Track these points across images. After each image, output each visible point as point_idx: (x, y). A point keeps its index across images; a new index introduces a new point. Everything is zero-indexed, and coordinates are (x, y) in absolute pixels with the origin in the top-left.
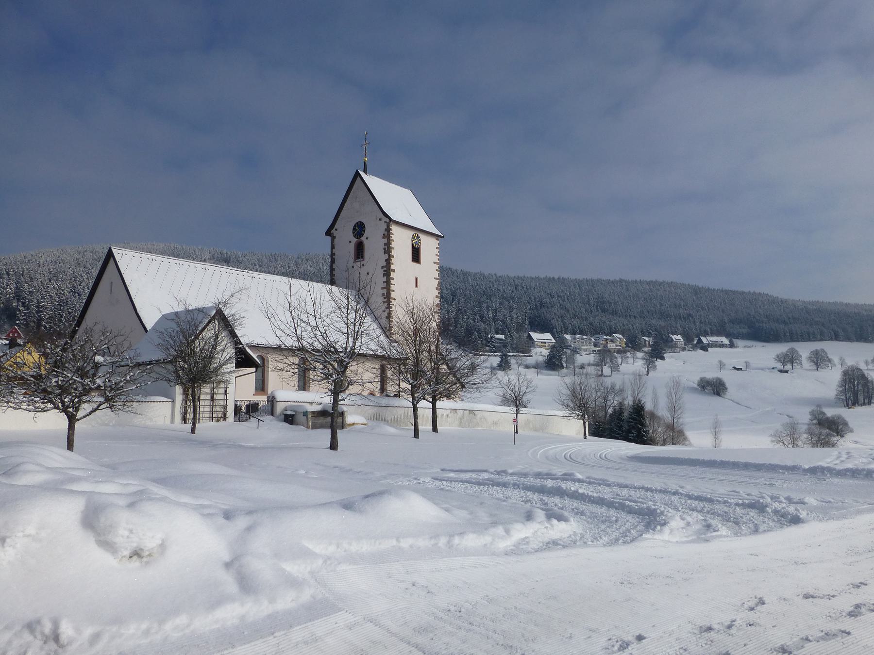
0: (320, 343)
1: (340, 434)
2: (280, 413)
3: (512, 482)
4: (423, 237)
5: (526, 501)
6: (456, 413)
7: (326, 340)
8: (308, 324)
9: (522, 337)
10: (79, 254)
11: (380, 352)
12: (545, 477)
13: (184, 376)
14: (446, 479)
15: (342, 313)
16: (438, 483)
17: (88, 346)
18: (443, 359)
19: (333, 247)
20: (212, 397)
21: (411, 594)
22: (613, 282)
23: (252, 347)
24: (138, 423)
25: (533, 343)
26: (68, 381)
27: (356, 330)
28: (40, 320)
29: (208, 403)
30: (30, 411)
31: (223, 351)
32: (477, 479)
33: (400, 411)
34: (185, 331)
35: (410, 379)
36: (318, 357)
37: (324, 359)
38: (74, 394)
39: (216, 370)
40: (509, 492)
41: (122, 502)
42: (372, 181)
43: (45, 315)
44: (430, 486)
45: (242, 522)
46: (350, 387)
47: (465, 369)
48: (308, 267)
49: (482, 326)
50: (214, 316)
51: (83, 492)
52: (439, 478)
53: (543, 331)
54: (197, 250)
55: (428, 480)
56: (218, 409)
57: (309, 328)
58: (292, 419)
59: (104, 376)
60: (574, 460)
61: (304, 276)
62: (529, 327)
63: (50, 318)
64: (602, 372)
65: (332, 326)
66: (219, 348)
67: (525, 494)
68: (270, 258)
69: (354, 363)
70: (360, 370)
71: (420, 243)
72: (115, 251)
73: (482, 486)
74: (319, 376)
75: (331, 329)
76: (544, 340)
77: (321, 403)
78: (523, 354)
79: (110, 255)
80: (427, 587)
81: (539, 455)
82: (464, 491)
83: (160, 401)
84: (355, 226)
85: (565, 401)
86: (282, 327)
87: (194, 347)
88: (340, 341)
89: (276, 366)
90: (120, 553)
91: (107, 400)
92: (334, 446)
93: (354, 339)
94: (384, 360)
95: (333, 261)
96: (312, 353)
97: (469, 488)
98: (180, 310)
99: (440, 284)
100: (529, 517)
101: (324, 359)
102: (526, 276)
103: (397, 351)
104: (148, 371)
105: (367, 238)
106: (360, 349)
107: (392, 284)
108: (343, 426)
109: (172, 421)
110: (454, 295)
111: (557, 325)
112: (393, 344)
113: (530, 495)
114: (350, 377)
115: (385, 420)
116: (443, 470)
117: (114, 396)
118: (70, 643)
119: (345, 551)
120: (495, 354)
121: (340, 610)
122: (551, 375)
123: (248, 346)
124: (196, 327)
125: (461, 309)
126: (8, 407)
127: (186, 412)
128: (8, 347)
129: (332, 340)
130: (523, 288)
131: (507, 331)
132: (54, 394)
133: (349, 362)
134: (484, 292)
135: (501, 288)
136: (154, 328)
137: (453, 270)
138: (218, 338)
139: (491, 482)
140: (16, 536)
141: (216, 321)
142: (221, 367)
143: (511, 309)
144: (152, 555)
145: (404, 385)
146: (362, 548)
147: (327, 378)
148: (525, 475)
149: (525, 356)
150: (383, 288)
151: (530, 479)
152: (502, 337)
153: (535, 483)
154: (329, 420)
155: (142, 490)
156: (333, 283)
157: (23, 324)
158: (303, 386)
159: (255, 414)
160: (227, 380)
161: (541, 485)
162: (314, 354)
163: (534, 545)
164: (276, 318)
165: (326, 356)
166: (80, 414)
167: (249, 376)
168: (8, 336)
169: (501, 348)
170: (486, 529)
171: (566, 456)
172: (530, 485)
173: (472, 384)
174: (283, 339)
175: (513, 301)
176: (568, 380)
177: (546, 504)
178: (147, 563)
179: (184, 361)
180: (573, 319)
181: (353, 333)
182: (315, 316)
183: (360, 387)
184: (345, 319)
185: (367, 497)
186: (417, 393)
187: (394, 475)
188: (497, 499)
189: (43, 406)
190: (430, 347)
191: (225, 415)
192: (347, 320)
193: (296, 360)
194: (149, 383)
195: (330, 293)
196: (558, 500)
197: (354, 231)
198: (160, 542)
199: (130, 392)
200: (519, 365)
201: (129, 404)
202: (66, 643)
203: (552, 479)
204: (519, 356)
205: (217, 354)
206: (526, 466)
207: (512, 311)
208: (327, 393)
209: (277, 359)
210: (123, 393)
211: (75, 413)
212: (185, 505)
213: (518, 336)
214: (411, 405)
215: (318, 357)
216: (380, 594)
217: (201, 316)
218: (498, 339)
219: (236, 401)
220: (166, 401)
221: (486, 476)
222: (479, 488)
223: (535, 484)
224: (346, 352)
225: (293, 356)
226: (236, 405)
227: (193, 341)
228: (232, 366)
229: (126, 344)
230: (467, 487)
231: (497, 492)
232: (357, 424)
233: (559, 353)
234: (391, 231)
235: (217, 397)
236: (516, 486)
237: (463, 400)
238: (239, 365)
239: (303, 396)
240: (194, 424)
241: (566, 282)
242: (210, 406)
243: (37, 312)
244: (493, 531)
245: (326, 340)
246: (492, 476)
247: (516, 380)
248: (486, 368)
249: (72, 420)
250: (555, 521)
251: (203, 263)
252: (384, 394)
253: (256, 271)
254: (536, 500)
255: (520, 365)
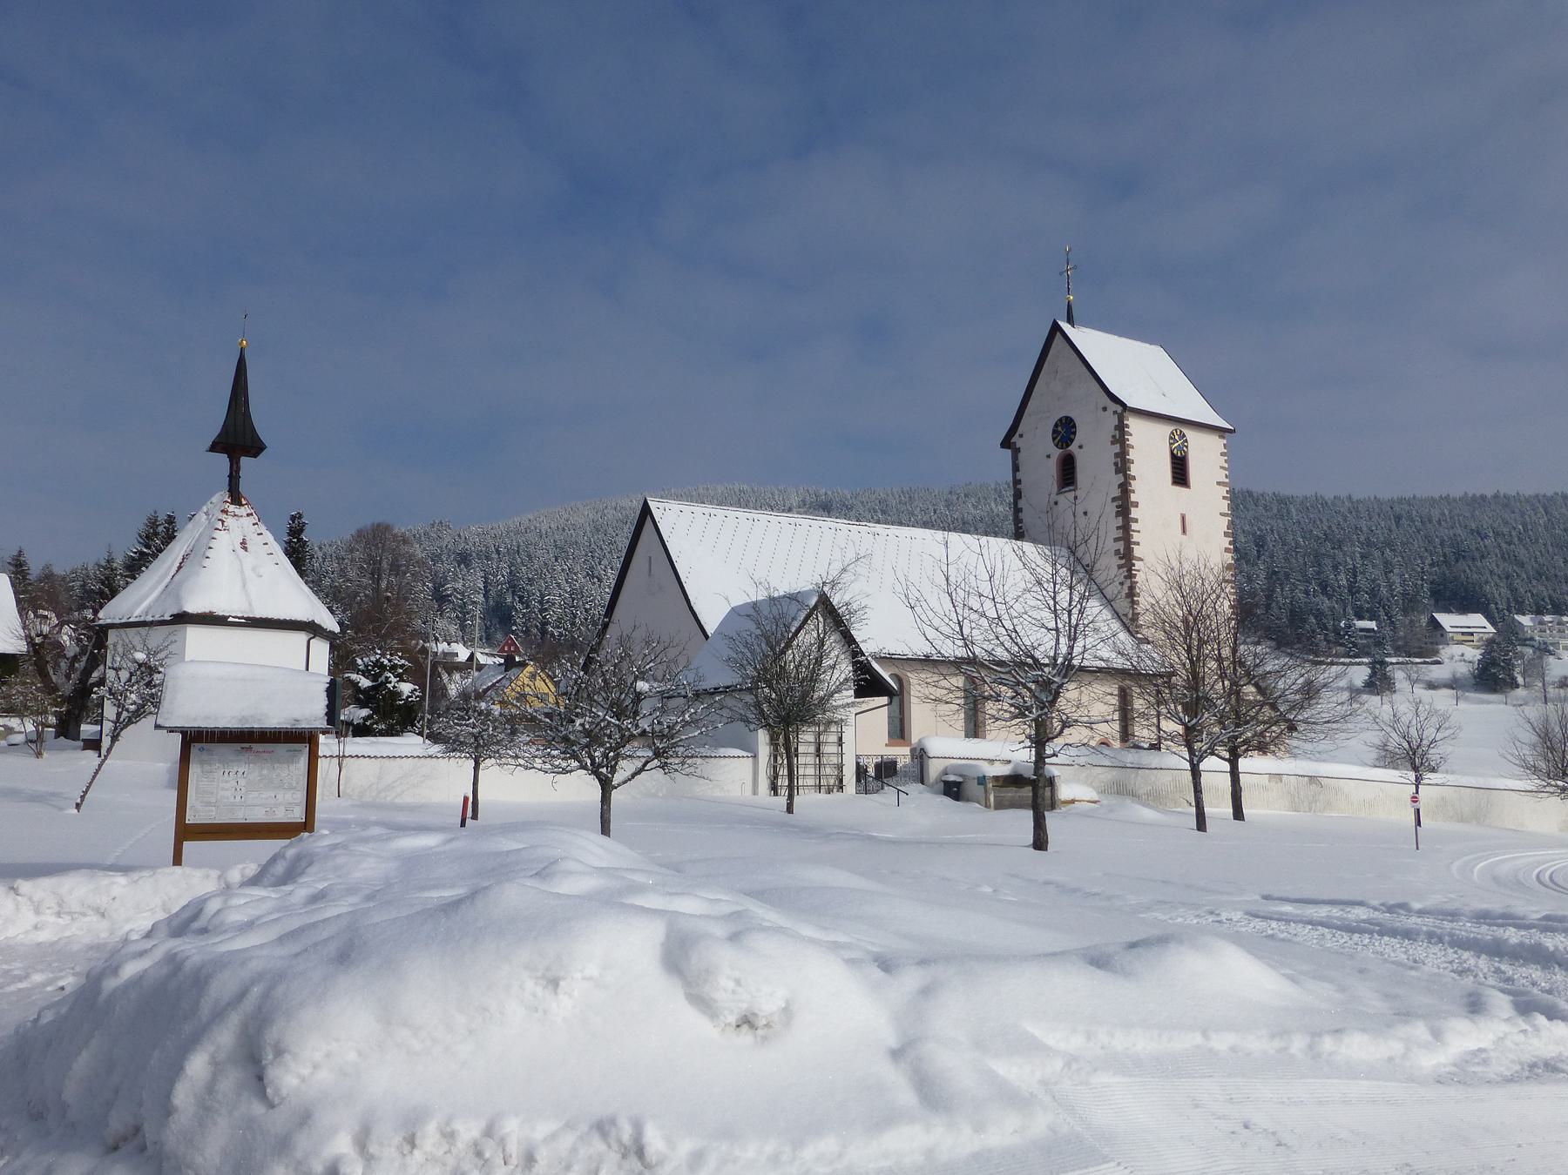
0: (1006, 649)
1: (1051, 820)
2: (936, 779)
3: (1425, 928)
4: (1190, 434)
5: (1462, 972)
6: (1281, 781)
7: (1017, 644)
8: (983, 615)
9: (1417, 625)
10: (597, 513)
11: (1119, 663)
12: (1500, 921)
13: (771, 713)
14: (1276, 916)
15: (1045, 593)
16: (1259, 924)
17: (625, 665)
18: (1248, 674)
19: (1016, 468)
20: (818, 750)
21: (1244, 1145)
23: (888, 660)
24: (701, 794)
25: (1442, 635)
26: (599, 724)
27: (1074, 622)
28: (545, 623)
29: (811, 760)
30: (547, 772)
31: (833, 667)
32: (1345, 919)
33: (1164, 778)
34: (769, 633)
35: (1181, 715)
36: (1003, 676)
37: (1015, 678)
38: (608, 745)
39: (823, 701)
40: (1419, 950)
41: (720, 930)
42: (1085, 338)
43: (551, 616)
44: (1243, 929)
45: (911, 979)
46: (1066, 731)
47: (1297, 692)
48: (970, 511)
49: (1325, 603)
50: (815, 607)
51: (663, 911)
52: (1262, 914)
53: (1464, 609)
54: (776, 492)
55: (1237, 916)
56: (828, 771)
57: (984, 622)
58: (959, 790)
59: (651, 714)
60: (1562, 888)
61: (964, 527)
62: (1432, 602)
63: (559, 620)
65: (1025, 616)
66: (826, 663)
67: (1456, 956)
68: (900, 496)
69: (1071, 686)
70: (1085, 699)
71: (1187, 447)
72: (652, 505)
73: (1357, 935)
74: (1006, 711)
75: (1025, 622)
76: (1469, 627)
77: (1010, 761)
78: (1422, 660)
79: (646, 512)
80: (1274, 1133)
81: (1475, 874)
82: (1317, 943)
83: (734, 757)
84: (1056, 425)
85: (1530, 759)
86: (936, 622)
87: (785, 662)
88: (1044, 645)
89: (927, 692)
90: (722, 1018)
91: (657, 754)
92: (1040, 843)
93: (1070, 640)
94: (1126, 679)
95: (1018, 495)
96: (993, 669)
97: (1329, 936)
98: (760, 598)
99: (1231, 524)
100: (1475, 1006)
101: (1015, 678)
102: (1418, 496)
103: (1153, 659)
104: (717, 705)
105: (1081, 447)
106: (1083, 658)
107: (1134, 531)
108: (1053, 806)
109: (755, 792)
110: (1260, 543)
111: (1497, 596)
112: (1144, 647)
113: (1468, 959)
114: (1066, 712)
115: (1133, 795)
116: (1266, 898)
117: (668, 747)
118: (660, 1163)
119: (1102, 1048)
120: (1358, 660)
121: (1105, 1159)
122: (1489, 702)
123: (875, 659)
124: (787, 627)
125: (1279, 572)
126: (517, 765)
127: (776, 776)
128: (503, 668)
129: (1028, 643)
130: (1413, 521)
131: (1382, 613)
132: (580, 744)
133: (1063, 684)
134: (1325, 534)
135: (1363, 524)
136: (718, 631)
137: (1255, 495)
138: (823, 646)
139: (1377, 928)
140: (572, 978)
141: (819, 615)
142: (832, 696)
143: (1388, 568)
144: (771, 1026)
145: (1170, 726)
146: (1134, 1045)
147: (1022, 715)
148: (1454, 915)
149: (1425, 663)
150: (1116, 540)
151: (1464, 925)
152: (1372, 625)
153: (1478, 934)
154: (1027, 792)
155: (739, 911)
156: (1019, 535)
157: (522, 631)
158: (975, 729)
159: (891, 781)
160: (842, 720)
161: (1493, 940)
162: (996, 671)
163: (1502, 1066)
164: (924, 604)
165: (1018, 674)
166: (617, 778)
167: (877, 712)
168: (502, 650)
169: (1369, 648)
170: (1389, 1026)
171: (1542, 878)
172: (1467, 937)
173: (1314, 723)
174: (938, 643)
175: (1391, 550)
176: (1534, 711)
177: (1509, 980)
178: (765, 1038)
179: (770, 687)
180: (1534, 582)
181: (1067, 628)
182: (994, 599)
183: (1086, 732)
184: (1051, 603)
185: (1133, 945)
186: (1198, 741)
187: (1165, 903)
188: (1393, 963)
189: (564, 764)
190: (1219, 650)
191: (841, 781)
192: (1055, 603)
193: (959, 681)
194: (720, 725)
195: (1021, 557)
196: (1539, 973)
197: (1055, 436)
198: (783, 1006)
199: (692, 741)
200: (1413, 682)
201: (689, 761)
202: (654, 1162)
203: (1519, 927)
204: (1412, 663)
205: (824, 673)
206: (1453, 896)
207: (1392, 571)
208: (1023, 742)
209: (929, 680)
210: (680, 743)
211: (610, 775)
212: (812, 941)
213: (1407, 622)
214: (1187, 766)
215: (1003, 676)
216: (1182, 1137)
217: (794, 606)
218: (1362, 630)
219: (858, 757)
220: (743, 757)
221: (1360, 913)
222: (1351, 939)
223: (1479, 936)
224: (1054, 665)
225: (956, 675)
226: (858, 763)
227: (783, 652)
228: (848, 694)
229: (682, 661)
230: (1323, 935)
231: (1394, 949)
232: (1080, 801)
233: (1508, 655)
234: (1126, 429)
235: (826, 749)
236: (1433, 937)
237: (1295, 756)
238: (860, 693)
239: (975, 748)
240: (791, 797)
241: (1513, 503)
242: (815, 765)
243: (541, 611)
244: (1404, 1030)
245: (1017, 644)
246: (1377, 915)
247: (1410, 715)
248: (1342, 689)
249: (606, 786)
250: (1541, 1020)
251: (786, 515)
252: (1129, 744)
253: (878, 522)
254: (1486, 970)
255: (1417, 681)
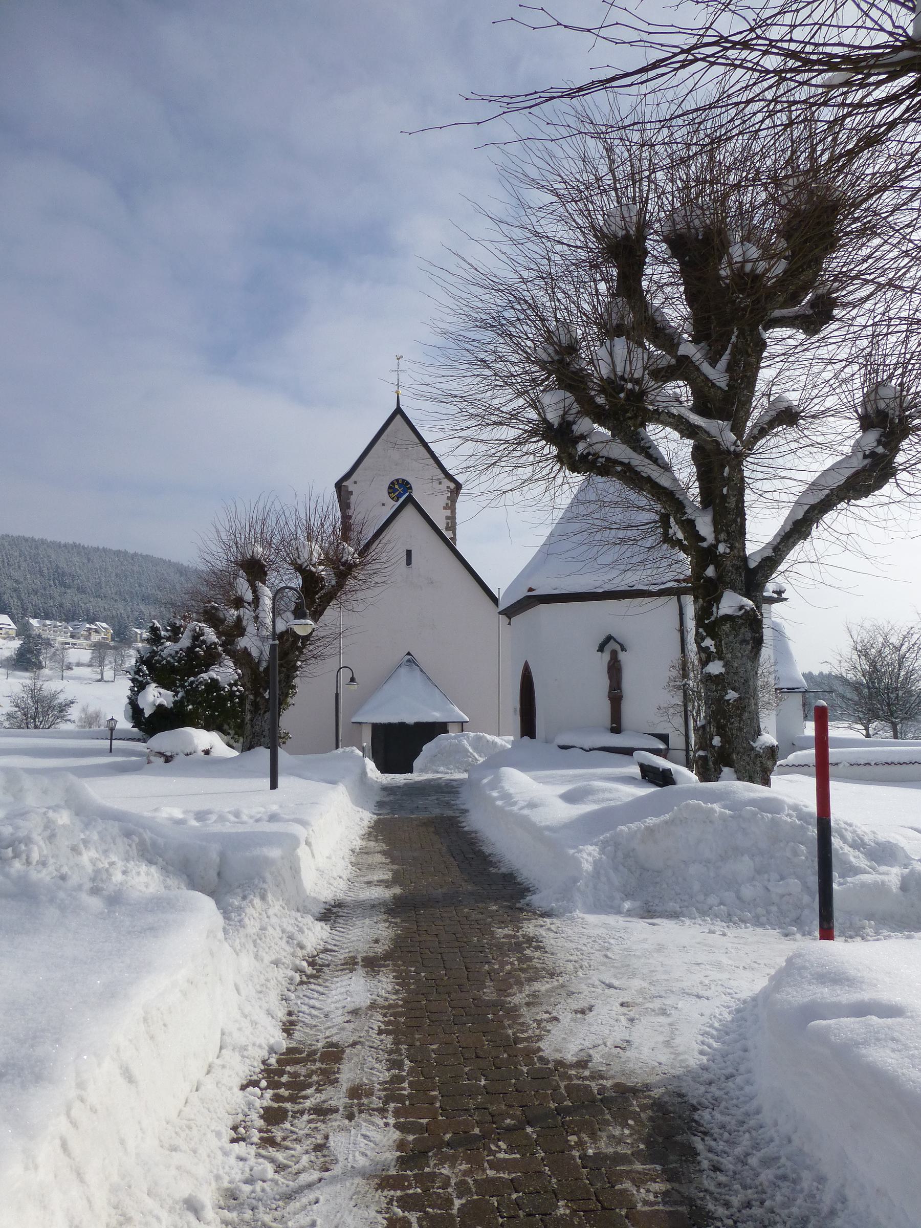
22: (65, 546)
64: (102, 675)
84: (392, 483)
